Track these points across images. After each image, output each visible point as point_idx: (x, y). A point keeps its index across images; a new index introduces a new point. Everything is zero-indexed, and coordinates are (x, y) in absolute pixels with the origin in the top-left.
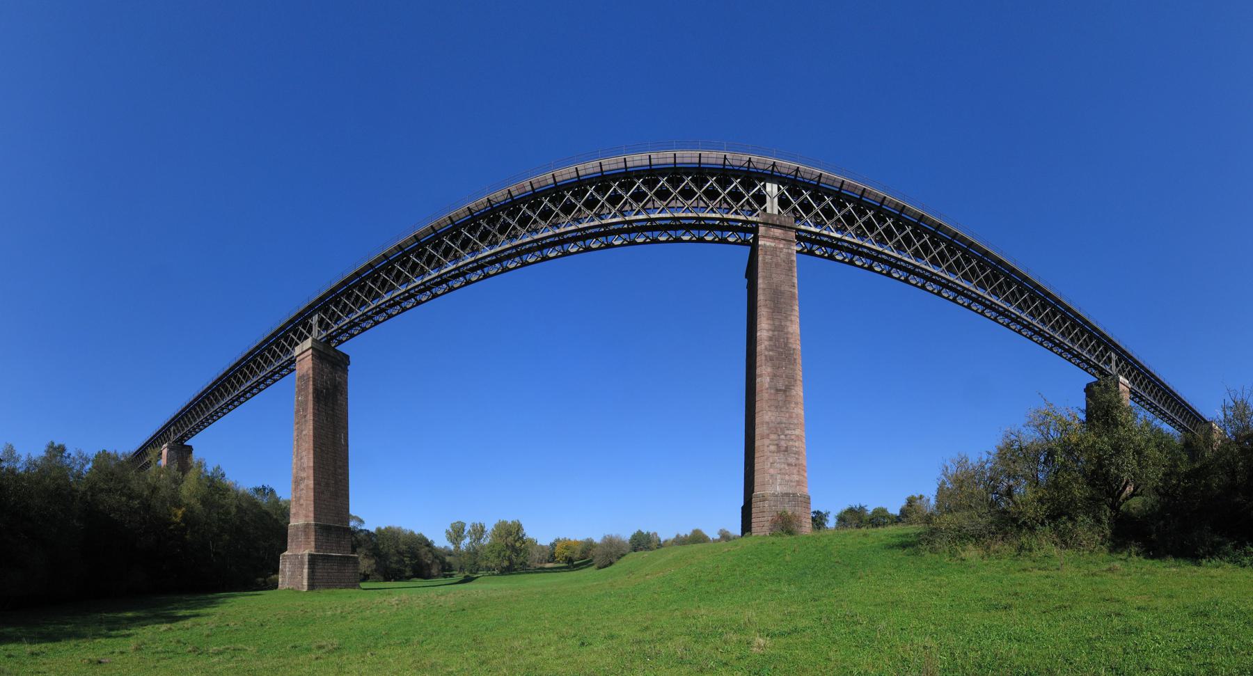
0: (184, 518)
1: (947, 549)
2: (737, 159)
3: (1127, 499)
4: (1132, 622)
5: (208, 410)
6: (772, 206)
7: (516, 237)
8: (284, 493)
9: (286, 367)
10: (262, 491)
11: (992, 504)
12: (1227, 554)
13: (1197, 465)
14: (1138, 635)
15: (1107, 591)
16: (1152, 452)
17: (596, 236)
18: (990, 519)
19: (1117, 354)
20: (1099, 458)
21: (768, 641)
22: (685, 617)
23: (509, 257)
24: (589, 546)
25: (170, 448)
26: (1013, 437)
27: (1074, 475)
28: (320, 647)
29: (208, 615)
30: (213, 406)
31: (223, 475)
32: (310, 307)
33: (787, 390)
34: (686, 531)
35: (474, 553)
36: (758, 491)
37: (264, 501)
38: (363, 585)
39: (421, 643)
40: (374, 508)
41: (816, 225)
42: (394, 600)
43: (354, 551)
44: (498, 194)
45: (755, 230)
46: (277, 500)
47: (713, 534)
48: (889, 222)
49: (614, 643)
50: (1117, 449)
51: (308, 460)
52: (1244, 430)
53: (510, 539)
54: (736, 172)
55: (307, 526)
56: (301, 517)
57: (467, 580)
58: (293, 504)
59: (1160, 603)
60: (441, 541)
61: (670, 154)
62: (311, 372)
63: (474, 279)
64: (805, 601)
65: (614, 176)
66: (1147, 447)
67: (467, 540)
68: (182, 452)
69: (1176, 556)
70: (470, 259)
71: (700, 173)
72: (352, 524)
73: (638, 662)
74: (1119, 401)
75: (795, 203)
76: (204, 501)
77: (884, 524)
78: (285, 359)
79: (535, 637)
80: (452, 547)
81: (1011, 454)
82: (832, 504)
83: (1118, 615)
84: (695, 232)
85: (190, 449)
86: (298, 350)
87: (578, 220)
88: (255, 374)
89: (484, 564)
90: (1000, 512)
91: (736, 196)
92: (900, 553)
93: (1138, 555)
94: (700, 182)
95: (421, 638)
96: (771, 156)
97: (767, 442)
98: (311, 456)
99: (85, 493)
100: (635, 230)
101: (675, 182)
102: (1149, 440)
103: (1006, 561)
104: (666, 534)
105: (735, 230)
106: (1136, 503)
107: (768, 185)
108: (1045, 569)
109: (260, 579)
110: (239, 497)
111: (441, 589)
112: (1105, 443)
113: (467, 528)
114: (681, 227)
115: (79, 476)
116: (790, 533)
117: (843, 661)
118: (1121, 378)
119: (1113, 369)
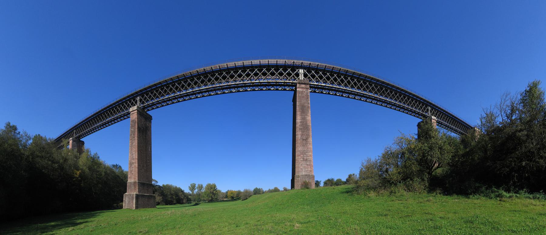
0: (80, 175)
1: (363, 193)
2: (290, 62)
3: (435, 169)
4: (437, 224)
5: (92, 126)
6: (301, 77)
7: (214, 84)
8: (125, 168)
9: (126, 115)
10: (116, 166)
11: (380, 176)
12: (482, 192)
13: (468, 150)
14: (440, 229)
15: (426, 209)
16: (447, 147)
17: (242, 87)
18: (379, 181)
19: (431, 107)
20: (423, 153)
21: (300, 225)
22: (272, 217)
23: (211, 91)
24: (239, 193)
25: (74, 141)
26: (388, 149)
27: (413, 161)
28: (140, 232)
29: (91, 221)
30: (94, 125)
31: (99, 157)
32: (136, 93)
33: (306, 140)
34: (272, 188)
35: (199, 195)
36: (296, 174)
37: (117, 171)
38: (158, 207)
39: (179, 228)
40: (161, 177)
41: (317, 82)
42: (169, 212)
43: (154, 193)
44: (208, 68)
45: (296, 86)
46: (122, 171)
47: (281, 189)
48: (342, 77)
49: (248, 226)
50: (431, 148)
51: (136, 156)
52: (491, 127)
53: (212, 190)
54: (289, 66)
55: (135, 182)
56: (132, 179)
57: (196, 204)
58: (129, 173)
59: (450, 215)
60: (187, 190)
61: (267, 61)
62: (136, 120)
63: (199, 96)
64: (313, 212)
65: (248, 67)
66: (444, 145)
67: (196, 190)
68: (79, 144)
69: (458, 194)
70: (197, 89)
71: (277, 67)
72: (153, 183)
73: (256, 232)
74: (432, 127)
75: (309, 75)
76: (90, 168)
77: (340, 185)
78: (126, 112)
79: (220, 224)
80: (191, 193)
81: (388, 156)
82: (322, 178)
83: (431, 220)
84: (275, 87)
85: (83, 143)
86: (131, 109)
87: (235, 81)
88: (113, 115)
89: (202, 199)
90: (382, 179)
91: (289, 74)
92: (346, 195)
93: (440, 194)
94: (277, 70)
95: (180, 226)
96: (301, 60)
97: (300, 157)
98: (137, 154)
99: (28, 156)
100: (255, 86)
101: (269, 70)
102: (445, 142)
103: (386, 197)
104: (265, 189)
105: (289, 86)
106: (439, 171)
107: (300, 70)
108: (401, 200)
109: (115, 205)
110: (106, 168)
111: (187, 208)
112: (426, 146)
113: (197, 186)
114: (271, 85)
115: (25, 146)
116: (308, 188)
117: (326, 232)
118: (433, 117)
119: (429, 114)
